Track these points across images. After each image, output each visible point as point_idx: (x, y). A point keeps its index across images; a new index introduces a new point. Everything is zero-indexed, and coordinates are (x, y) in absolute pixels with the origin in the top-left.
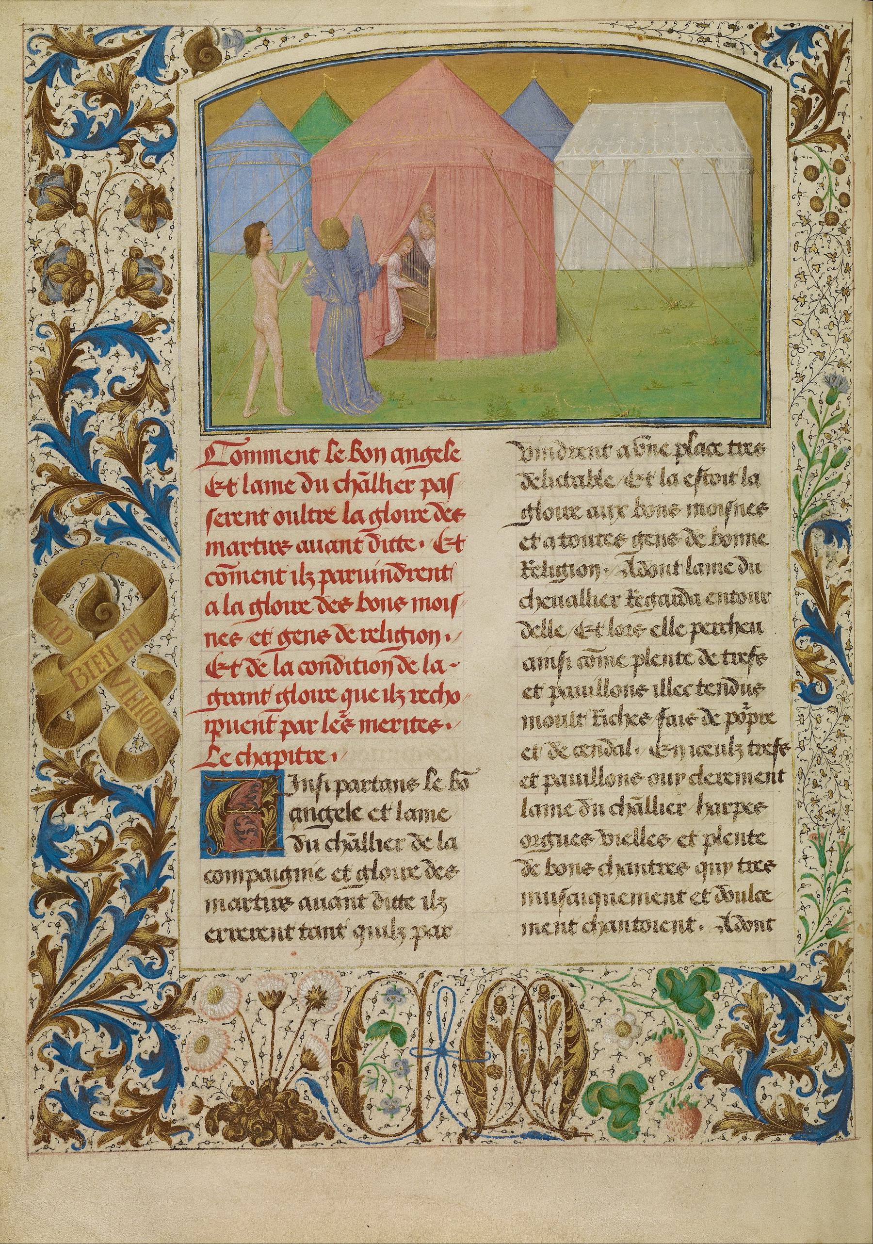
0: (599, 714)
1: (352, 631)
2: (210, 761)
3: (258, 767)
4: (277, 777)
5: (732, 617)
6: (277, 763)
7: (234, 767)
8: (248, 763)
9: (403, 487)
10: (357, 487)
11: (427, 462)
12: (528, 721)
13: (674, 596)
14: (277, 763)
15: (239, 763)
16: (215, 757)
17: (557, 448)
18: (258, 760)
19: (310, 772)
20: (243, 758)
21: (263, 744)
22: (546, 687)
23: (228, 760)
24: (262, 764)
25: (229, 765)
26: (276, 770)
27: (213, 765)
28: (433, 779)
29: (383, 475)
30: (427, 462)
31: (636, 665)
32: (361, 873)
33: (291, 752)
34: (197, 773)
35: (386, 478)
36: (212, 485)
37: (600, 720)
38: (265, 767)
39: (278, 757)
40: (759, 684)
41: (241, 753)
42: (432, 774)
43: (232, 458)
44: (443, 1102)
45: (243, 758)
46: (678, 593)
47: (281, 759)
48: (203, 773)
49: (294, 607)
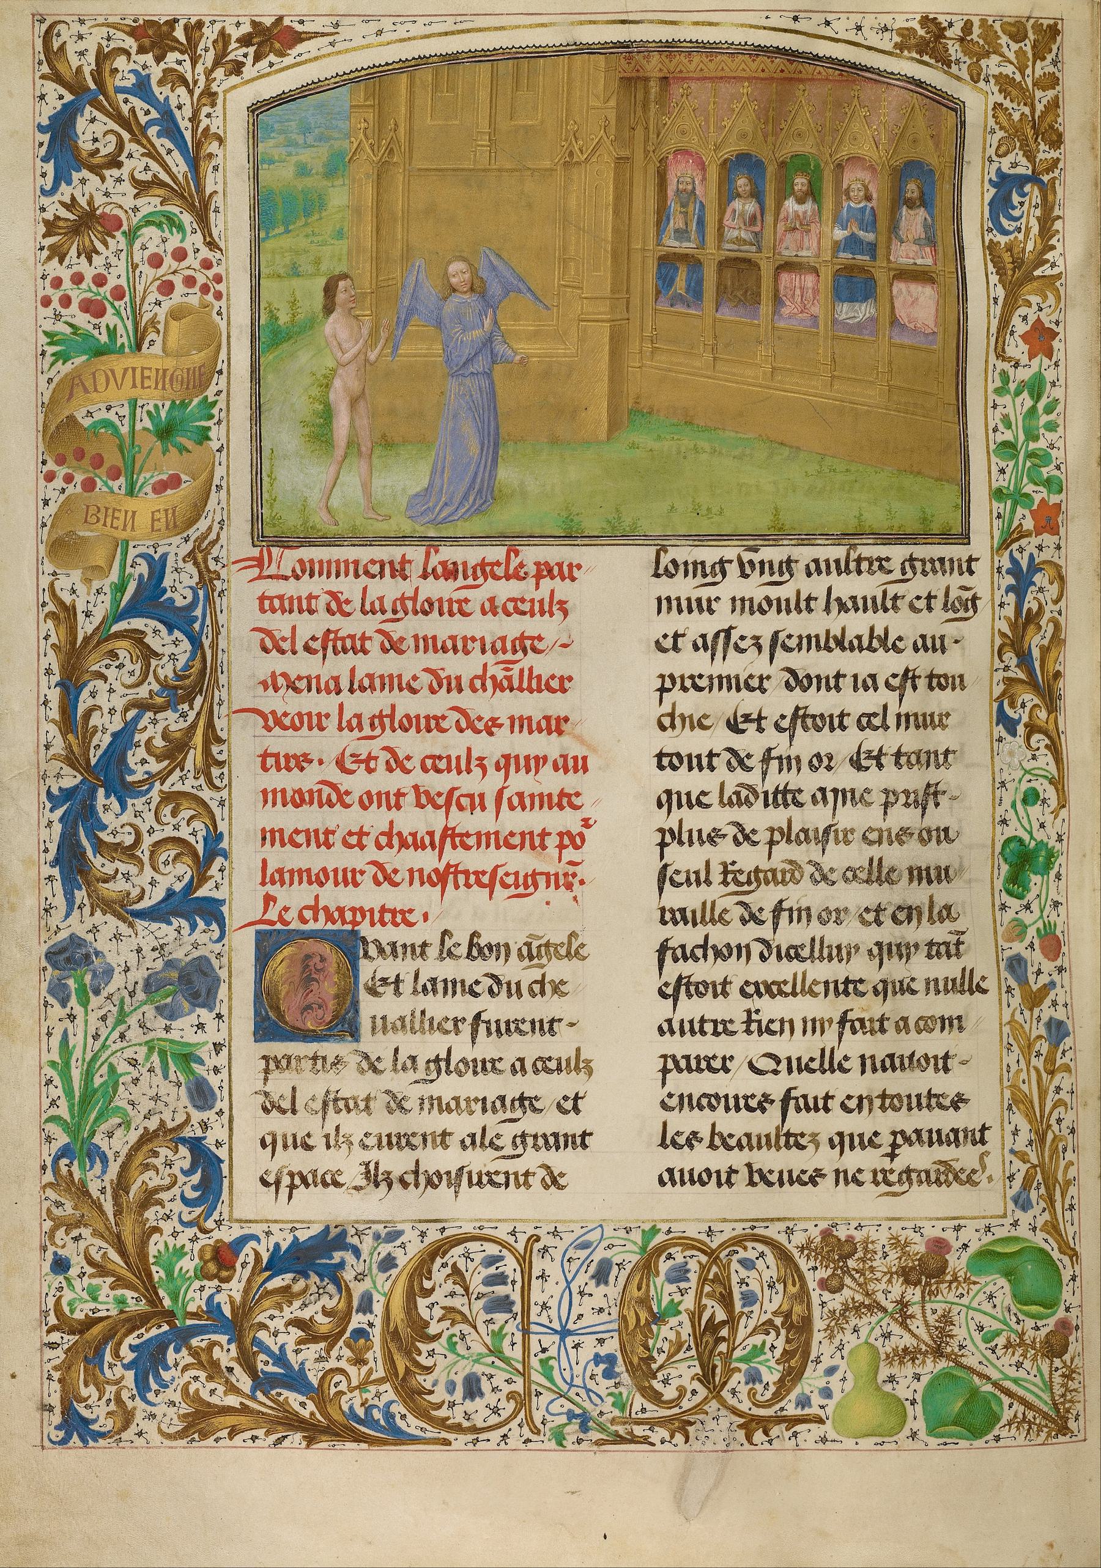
0: (730, 868)
1: (408, 758)
2: (266, 917)
3: (330, 926)
6: (355, 923)
7: (295, 925)
8: (316, 920)
9: (555, 684)
10: (403, 844)
11: (481, 580)
12: (387, 680)
16: (272, 914)
20: (308, 914)
21: (333, 896)
23: (287, 917)
24: (334, 923)
27: (272, 923)
28: (449, 943)
29: (531, 669)
30: (481, 580)
31: (772, 843)
33: (372, 911)
34: (251, 931)
35: (535, 674)
37: (754, 1027)
38: (338, 926)
39: (354, 915)
43: (294, 571)
44: (568, 1283)
45: (308, 914)
48: (258, 932)
49: (698, 1063)
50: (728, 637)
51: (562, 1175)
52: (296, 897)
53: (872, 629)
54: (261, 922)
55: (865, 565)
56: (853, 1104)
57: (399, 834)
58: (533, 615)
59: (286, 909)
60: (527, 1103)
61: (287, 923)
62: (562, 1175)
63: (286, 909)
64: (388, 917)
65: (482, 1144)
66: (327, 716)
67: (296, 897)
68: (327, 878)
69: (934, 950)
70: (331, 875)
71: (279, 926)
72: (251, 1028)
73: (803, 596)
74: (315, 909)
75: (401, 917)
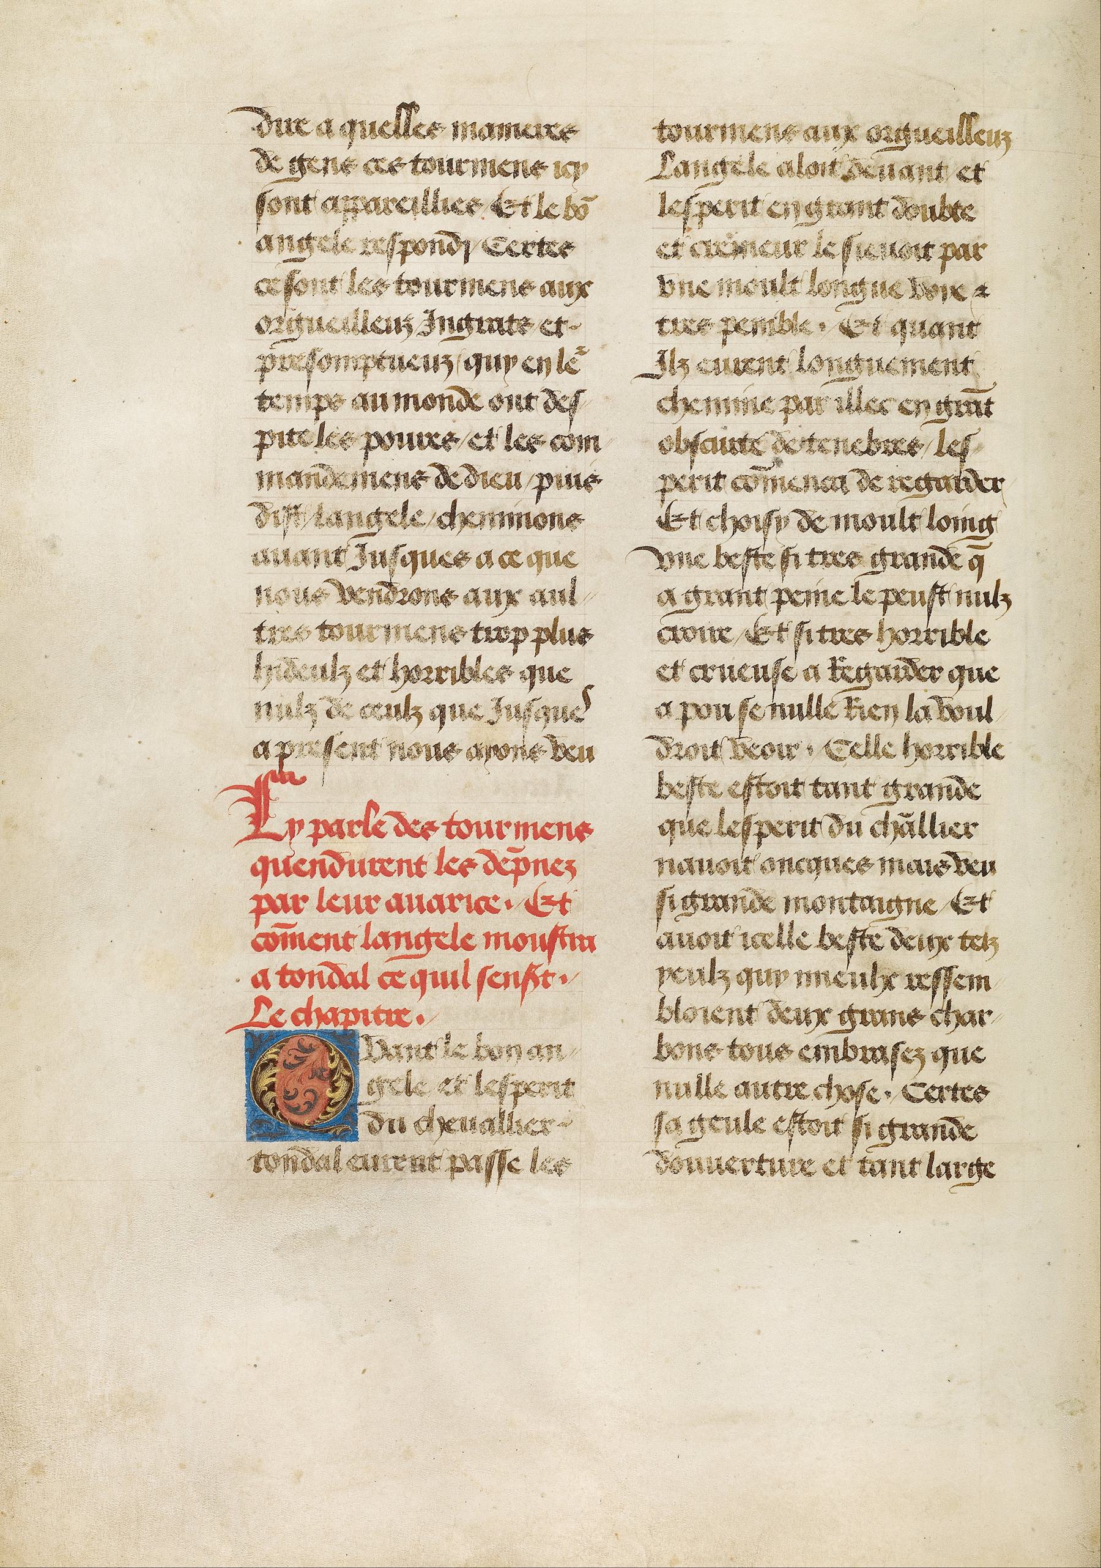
3: (323, 1027)
4: (347, 1042)
5: (830, 1078)
7: (290, 1026)
8: (308, 1021)
13: (897, 668)
14: (347, 1022)
15: (296, 1022)
16: (264, 1016)
17: (750, 897)
18: (322, 1018)
19: (393, 1035)
20: (301, 1017)
21: (326, 999)
22: (807, 783)
23: (281, 1019)
25: (281, 1025)
26: (345, 1030)
31: (886, 603)
32: (689, 900)
34: (241, 1033)
36: (667, 516)
38: (331, 1027)
40: (451, 434)
41: (300, 1010)
42: (263, 1006)
45: (301, 1017)
46: (902, 664)
47: (352, 1017)
48: (249, 1034)
50: (948, 978)
51: (970, 1128)
52: (289, 999)
53: (464, 660)
54: (250, 1024)
55: (782, 1090)
56: (533, 365)
57: (318, 1010)
58: (348, 911)
59: (280, 1012)
60: (959, 1093)
61: (281, 1025)
62: (970, 1128)
63: (280, 1012)
64: (383, 1017)
65: (747, 1128)
66: (305, 899)
67: (289, 999)
68: (874, 523)
69: (554, 403)
70: (879, 520)
71: (271, 1028)
72: (243, 1121)
73: (907, 515)
74: (307, 1011)
75: (398, 1018)
